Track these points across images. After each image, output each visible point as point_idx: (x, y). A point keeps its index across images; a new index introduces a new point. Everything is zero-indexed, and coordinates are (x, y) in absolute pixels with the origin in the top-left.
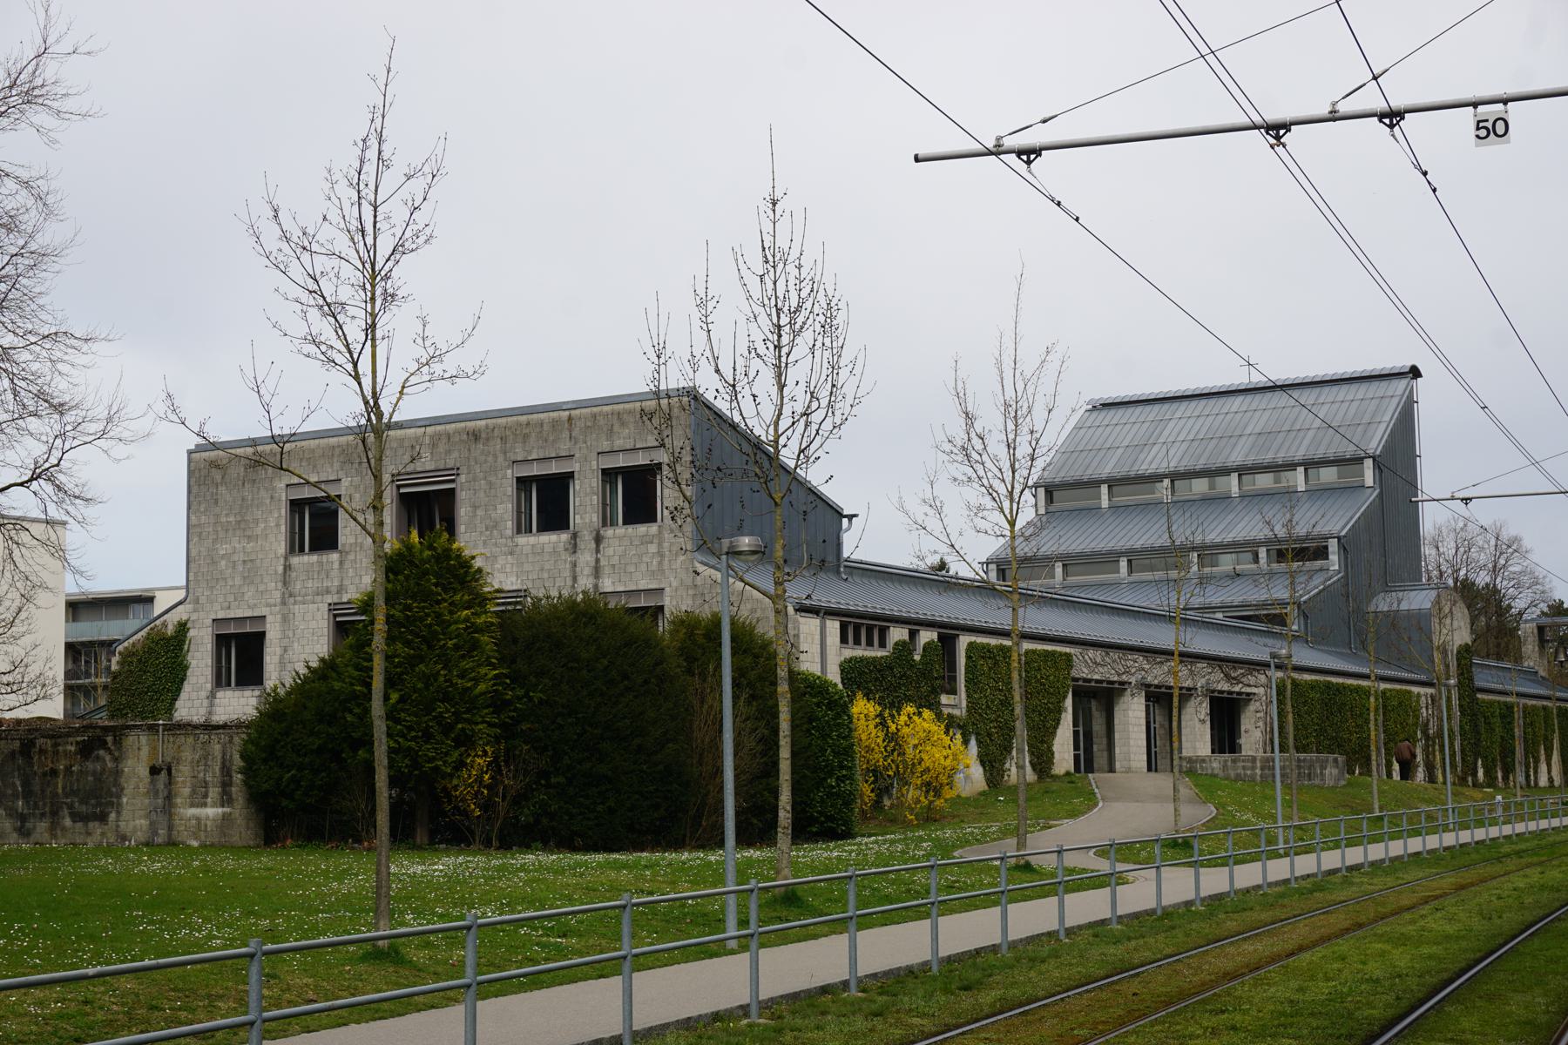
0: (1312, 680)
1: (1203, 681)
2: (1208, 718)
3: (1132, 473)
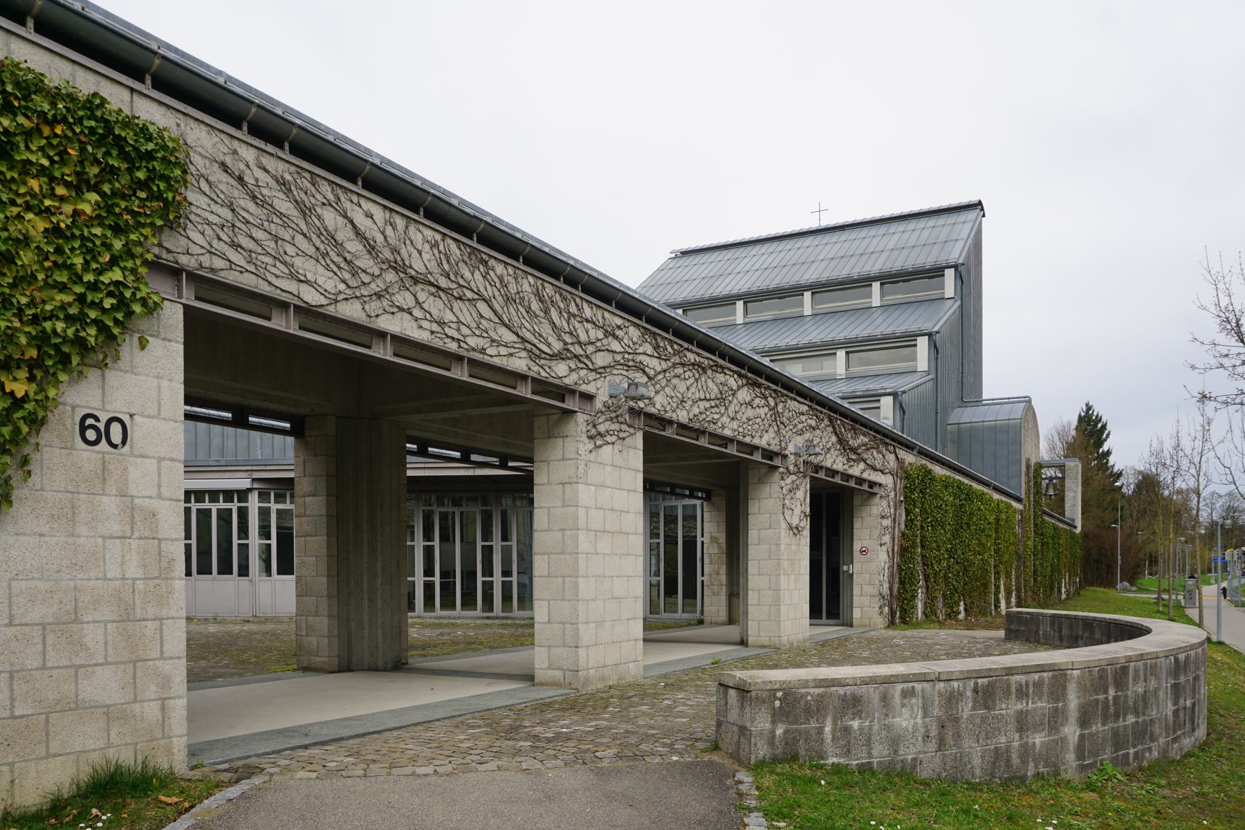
0: (947, 477)
1: (799, 441)
2: (806, 524)
3: (707, 296)
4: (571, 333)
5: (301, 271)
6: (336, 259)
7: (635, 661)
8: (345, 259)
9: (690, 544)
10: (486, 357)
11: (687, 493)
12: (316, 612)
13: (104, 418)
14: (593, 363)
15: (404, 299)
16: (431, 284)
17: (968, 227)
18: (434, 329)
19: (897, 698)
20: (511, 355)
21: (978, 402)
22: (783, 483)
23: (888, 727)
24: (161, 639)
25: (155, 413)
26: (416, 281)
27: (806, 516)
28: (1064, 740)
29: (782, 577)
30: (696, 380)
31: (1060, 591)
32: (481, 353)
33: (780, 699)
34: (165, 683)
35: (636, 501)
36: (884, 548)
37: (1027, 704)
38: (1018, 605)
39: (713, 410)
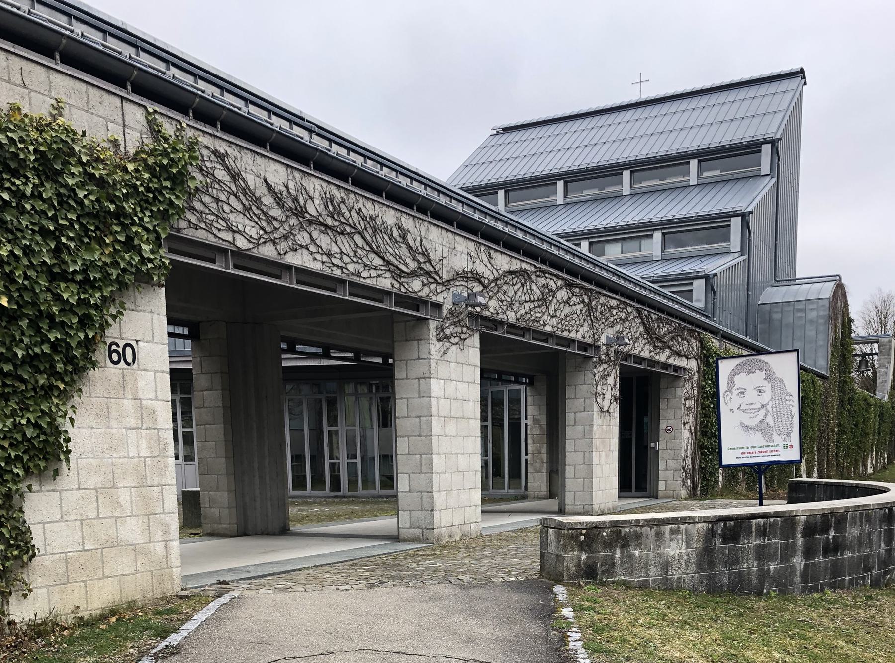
1: (610, 332)
2: (615, 410)
4: (423, 254)
5: (234, 224)
6: (256, 211)
7: (476, 522)
8: (262, 211)
9: (515, 426)
10: (362, 280)
11: (512, 379)
12: (218, 488)
13: (122, 344)
14: (440, 278)
15: (302, 238)
16: (322, 224)
17: (789, 96)
18: (324, 260)
19: (667, 535)
20: (379, 276)
21: (791, 280)
22: (595, 371)
23: (660, 555)
24: (163, 499)
25: (151, 339)
26: (310, 222)
27: (615, 399)
28: (792, 567)
29: (594, 453)
30: (522, 285)
31: (865, 466)
32: (358, 276)
33: (584, 535)
34: (166, 532)
35: (475, 392)
36: (687, 426)
37: (764, 540)
38: (820, 477)
39: (536, 310)
